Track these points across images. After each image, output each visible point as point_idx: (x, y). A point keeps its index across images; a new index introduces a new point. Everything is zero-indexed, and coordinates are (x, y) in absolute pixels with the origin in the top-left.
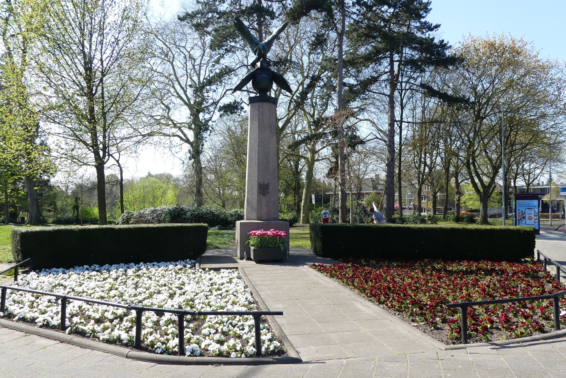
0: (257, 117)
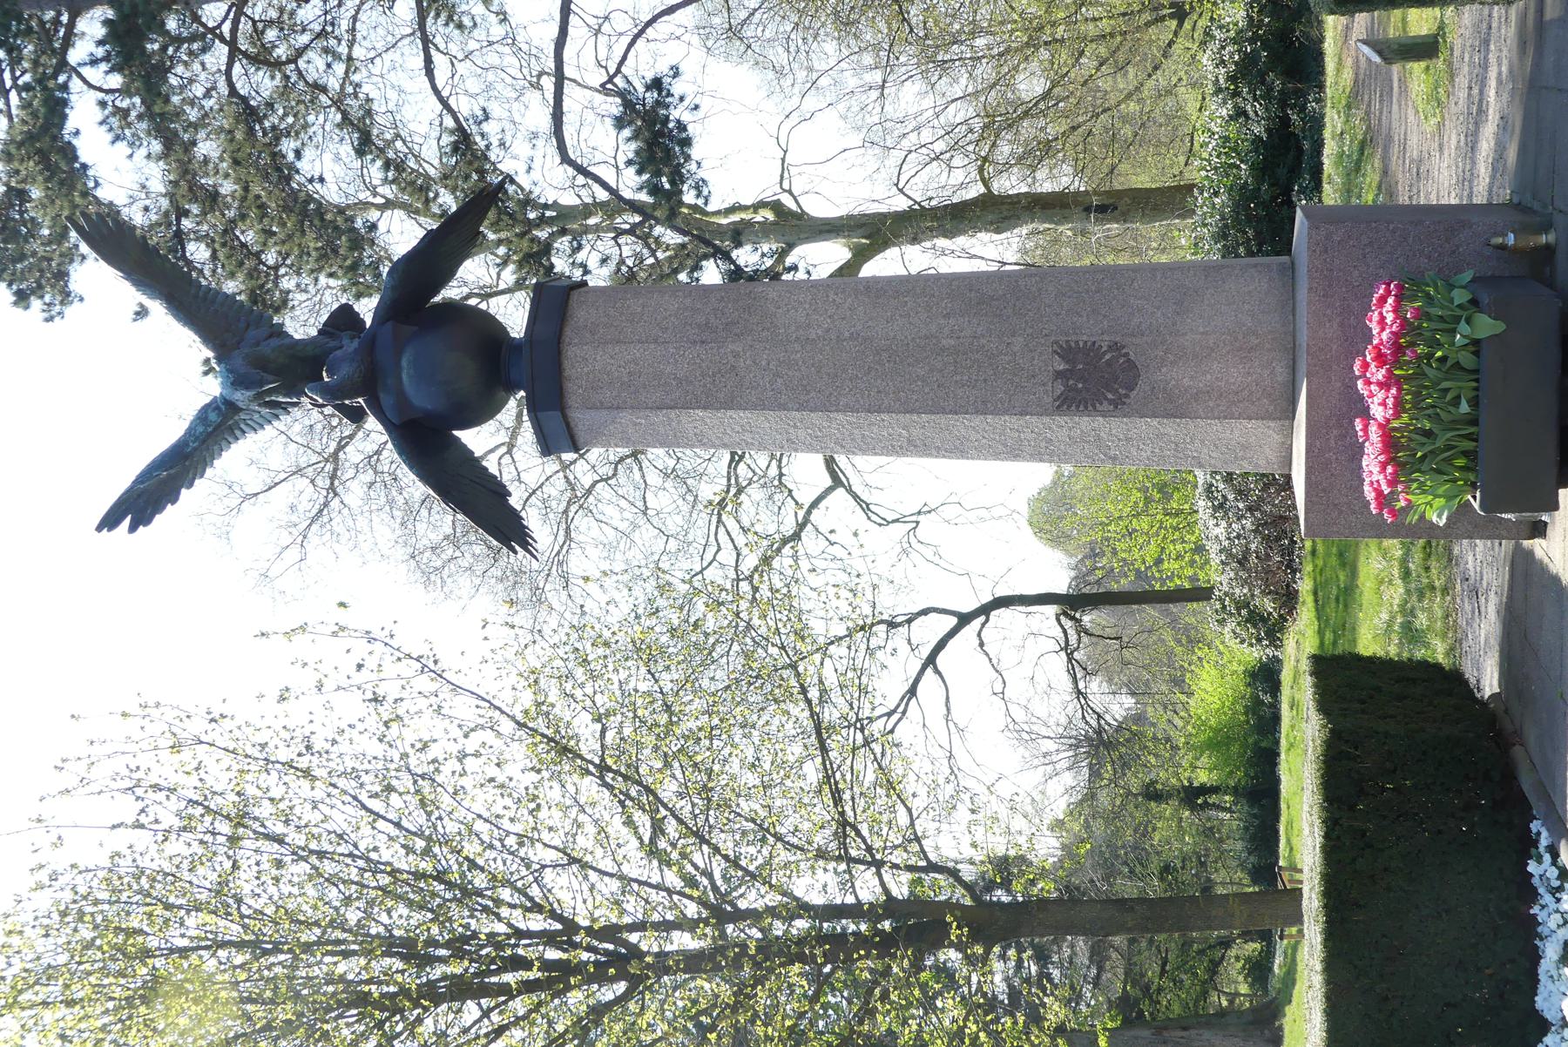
0: (658, 417)
